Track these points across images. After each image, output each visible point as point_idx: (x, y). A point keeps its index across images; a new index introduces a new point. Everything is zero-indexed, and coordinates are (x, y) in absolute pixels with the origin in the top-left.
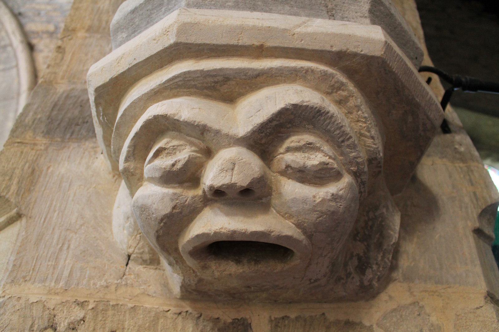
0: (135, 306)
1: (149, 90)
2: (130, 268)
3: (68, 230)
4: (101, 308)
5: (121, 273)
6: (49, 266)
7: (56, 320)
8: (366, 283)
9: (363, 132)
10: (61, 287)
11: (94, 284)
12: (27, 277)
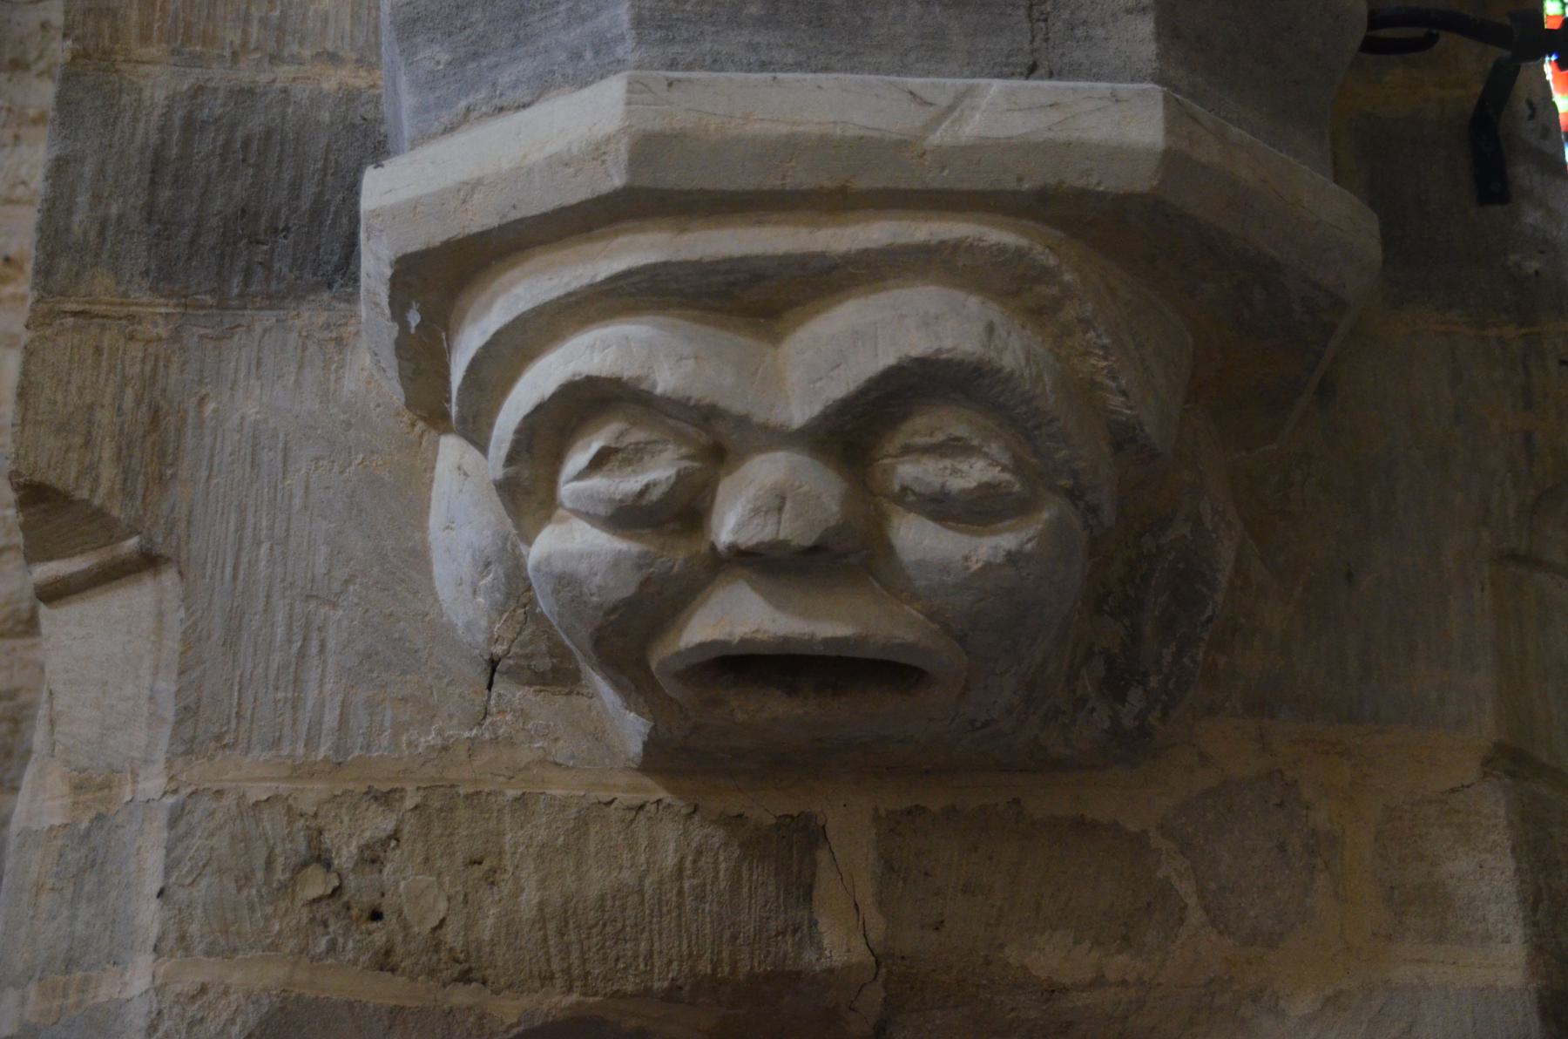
0: (524, 794)
1: (561, 291)
2: (499, 695)
3: (309, 597)
4: (438, 805)
5: (478, 708)
6: (281, 704)
7: (328, 841)
8: (1128, 723)
9: (1099, 379)
10: (326, 760)
11: (409, 744)
12: (227, 737)
